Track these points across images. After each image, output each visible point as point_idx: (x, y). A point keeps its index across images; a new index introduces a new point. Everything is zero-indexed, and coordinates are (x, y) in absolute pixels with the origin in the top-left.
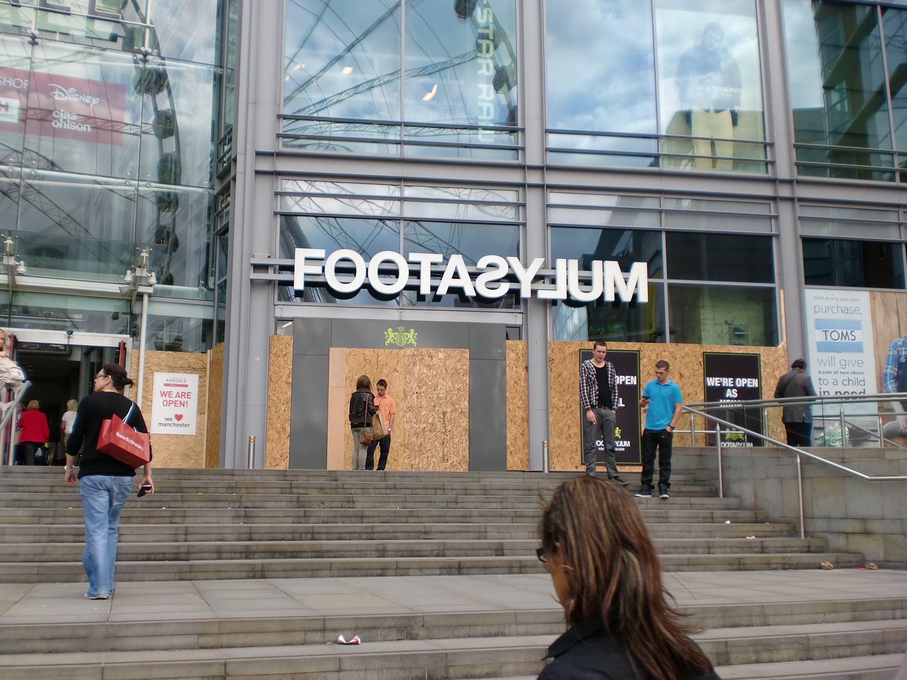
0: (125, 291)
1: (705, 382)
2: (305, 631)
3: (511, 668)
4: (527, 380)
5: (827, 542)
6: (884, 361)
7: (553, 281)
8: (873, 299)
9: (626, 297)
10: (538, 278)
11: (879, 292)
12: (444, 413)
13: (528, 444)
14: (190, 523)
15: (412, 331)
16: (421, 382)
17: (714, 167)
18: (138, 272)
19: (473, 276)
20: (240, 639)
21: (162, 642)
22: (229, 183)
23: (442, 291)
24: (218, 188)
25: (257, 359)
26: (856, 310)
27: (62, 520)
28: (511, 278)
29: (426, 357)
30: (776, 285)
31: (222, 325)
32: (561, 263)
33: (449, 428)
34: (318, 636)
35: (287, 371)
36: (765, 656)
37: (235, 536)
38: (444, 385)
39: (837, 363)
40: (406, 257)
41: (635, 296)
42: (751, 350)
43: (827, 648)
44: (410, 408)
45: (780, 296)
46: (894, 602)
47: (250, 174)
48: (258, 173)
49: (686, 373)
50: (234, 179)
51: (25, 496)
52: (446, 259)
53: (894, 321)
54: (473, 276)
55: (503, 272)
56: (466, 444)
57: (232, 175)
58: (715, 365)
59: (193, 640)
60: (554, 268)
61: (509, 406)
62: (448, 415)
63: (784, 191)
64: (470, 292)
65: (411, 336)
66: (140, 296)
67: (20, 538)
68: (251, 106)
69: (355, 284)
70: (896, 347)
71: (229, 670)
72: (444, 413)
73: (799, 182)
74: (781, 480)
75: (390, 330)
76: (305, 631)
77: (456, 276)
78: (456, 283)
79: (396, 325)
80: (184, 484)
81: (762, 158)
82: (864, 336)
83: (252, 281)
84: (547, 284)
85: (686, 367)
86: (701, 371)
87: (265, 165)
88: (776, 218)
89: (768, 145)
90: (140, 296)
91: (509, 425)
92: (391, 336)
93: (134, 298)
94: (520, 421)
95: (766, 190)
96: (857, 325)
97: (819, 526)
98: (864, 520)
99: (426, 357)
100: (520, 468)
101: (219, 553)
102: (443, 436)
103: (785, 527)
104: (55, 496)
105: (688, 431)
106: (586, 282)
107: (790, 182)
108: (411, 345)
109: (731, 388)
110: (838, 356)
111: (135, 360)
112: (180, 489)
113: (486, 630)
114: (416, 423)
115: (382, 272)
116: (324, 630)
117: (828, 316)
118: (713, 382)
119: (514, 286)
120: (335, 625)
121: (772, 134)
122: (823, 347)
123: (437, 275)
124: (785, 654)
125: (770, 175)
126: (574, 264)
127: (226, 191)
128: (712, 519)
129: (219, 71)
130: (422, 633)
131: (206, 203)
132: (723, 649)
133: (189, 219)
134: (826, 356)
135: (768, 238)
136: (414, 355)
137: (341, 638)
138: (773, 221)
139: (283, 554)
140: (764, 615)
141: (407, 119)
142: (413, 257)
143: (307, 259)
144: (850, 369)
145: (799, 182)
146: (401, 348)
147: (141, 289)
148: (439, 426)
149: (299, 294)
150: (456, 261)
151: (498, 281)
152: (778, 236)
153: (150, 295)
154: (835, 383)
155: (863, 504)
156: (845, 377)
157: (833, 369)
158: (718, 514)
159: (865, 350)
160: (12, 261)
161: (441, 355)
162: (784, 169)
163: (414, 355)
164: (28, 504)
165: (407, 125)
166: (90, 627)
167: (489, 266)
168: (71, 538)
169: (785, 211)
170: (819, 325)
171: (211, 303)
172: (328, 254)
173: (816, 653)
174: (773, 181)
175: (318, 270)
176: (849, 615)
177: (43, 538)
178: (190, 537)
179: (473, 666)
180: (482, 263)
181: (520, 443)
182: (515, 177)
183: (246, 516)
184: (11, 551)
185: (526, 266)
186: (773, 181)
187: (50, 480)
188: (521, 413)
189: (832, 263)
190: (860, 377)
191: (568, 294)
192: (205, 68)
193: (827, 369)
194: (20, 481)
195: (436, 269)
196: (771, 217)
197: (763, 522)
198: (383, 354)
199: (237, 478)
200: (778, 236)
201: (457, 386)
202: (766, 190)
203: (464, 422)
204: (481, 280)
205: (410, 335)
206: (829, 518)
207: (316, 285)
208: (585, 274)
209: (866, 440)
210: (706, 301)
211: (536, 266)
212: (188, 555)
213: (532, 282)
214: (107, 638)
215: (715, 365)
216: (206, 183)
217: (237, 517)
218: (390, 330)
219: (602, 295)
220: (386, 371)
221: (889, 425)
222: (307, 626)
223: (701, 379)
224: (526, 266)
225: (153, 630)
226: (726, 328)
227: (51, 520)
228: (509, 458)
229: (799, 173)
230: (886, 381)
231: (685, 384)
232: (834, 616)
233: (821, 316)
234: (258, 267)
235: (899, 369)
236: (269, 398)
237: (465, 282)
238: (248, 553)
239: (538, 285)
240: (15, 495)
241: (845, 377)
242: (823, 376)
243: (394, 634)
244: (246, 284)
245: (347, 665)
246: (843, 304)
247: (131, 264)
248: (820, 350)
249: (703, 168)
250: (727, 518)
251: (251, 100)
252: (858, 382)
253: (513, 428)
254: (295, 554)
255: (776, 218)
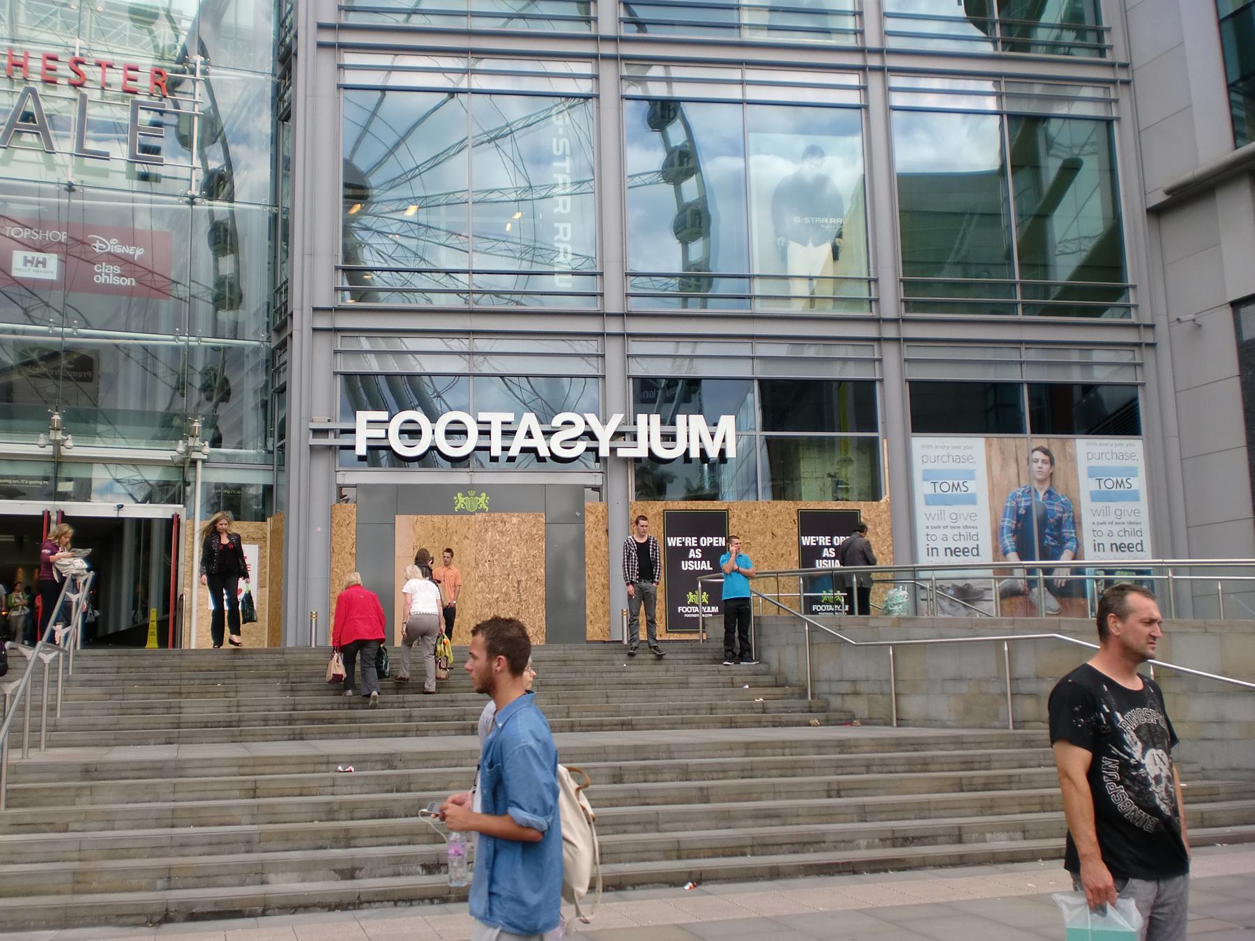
0: (176, 460)
1: (800, 541)
2: (315, 764)
3: (456, 784)
4: (607, 544)
5: (827, 702)
6: (1001, 514)
7: (635, 438)
8: (989, 445)
9: (713, 453)
10: (617, 435)
11: (995, 438)
12: (519, 582)
13: (608, 613)
14: (242, 697)
15: (484, 495)
16: (493, 549)
17: (812, 307)
18: (191, 442)
19: (548, 434)
20: (268, 769)
21: (215, 771)
22: (285, 340)
23: (514, 452)
24: (275, 342)
25: (319, 529)
26: (969, 459)
27: (131, 696)
28: (590, 435)
29: (499, 523)
30: (879, 434)
31: (279, 494)
32: (642, 418)
33: (524, 597)
34: (324, 767)
35: (351, 542)
36: (651, 777)
37: (280, 707)
38: (518, 552)
39: (947, 516)
40: (475, 416)
41: (722, 452)
42: (850, 506)
43: (703, 772)
44: (482, 578)
45: (884, 446)
46: (784, 742)
47: (307, 332)
48: (315, 330)
49: (779, 532)
50: (291, 335)
51: (95, 676)
52: (519, 418)
53: (1013, 470)
54: (548, 434)
55: (579, 429)
56: (542, 614)
57: (288, 332)
58: (811, 522)
59: (235, 770)
60: (635, 423)
61: (589, 572)
62: (523, 584)
63: (890, 331)
64: (544, 453)
65: (483, 500)
66: (194, 462)
67: (96, 712)
68: (307, 258)
69: (420, 448)
70: (1014, 497)
71: (258, 785)
72: (519, 582)
73: (905, 320)
74: (797, 646)
75: (460, 495)
76: (315, 764)
77: (529, 435)
78: (529, 443)
79: (465, 489)
80: (237, 662)
81: (866, 296)
82: (979, 486)
83: (312, 448)
84: (629, 442)
85: (779, 526)
86: (796, 530)
87: (323, 322)
88: (880, 360)
89: (872, 281)
90: (194, 462)
91: (588, 592)
92: (461, 501)
93: (187, 465)
94: (600, 588)
95: (870, 331)
96: (970, 475)
97: (823, 688)
98: (854, 682)
99: (499, 523)
100: (601, 638)
101: (266, 721)
102: (518, 606)
103: (796, 690)
104: (122, 676)
105: (775, 596)
106: (669, 438)
107: (896, 321)
108: (483, 510)
109: (828, 547)
110: (949, 509)
111: (189, 532)
112: (234, 668)
113: (448, 763)
114: (489, 593)
115: (448, 433)
116: (328, 763)
117: (938, 466)
118: (808, 541)
119: (592, 444)
120: (336, 759)
121: (876, 268)
122: (930, 500)
123: (508, 433)
124: (667, 776)
125: (874, 314)
126: (656, 419)
127: (283, 346)
128: (732, 684)
129: (274, 210)
130: (400, 765)
131: (263, 356)
132: (617, 772)
133: (246, 370)
134: (934, 509)
135: (870, 384)
136: (485, 521)
137: (340, 768)
138: (877, 364)
139: (322, 721)
140: (670, 751)
141: (475, 268)
142: (483, 417)
143: (369, 422)
144: (961, 523)
145: (905, 320)
146: (473, 514)
147: (195, 455)
148: (514, 596)
149: (361, 458)
150: (529, 420)
151: (576, 439)
152: (881, 381)
153: (204, 461)
154: (945, 538)
155: (855, 667)
156: (956, 531)
157: (942, 523)
158: (737, 679)
159: (978, 501)
160: (59, 436)
161: (515, 520)
162: (890, 306)
163: (485, 521)
164: (99, 683)
165: (474, 272)
166: (165, 761)
167: (564, 423)
168: (140, 711)
169: (891, 354)
170: (927, 476)
171: (270, 467)
172: (391, 417)
173: (694, 776)
174: (878, 321)
175: (382, 434)
176: (743, 752)
177: (116, 712)
178: (242, 709)
179: (429, 783)
180: (557, 421)
181: (600, 611)
182: (593, 326)
183: (292, 690)
184: (91, 722)
185: (605, 422)
186: (878, 321)
187: (115, 662)
188: (601, 580)
189: (941, 409)
190: (973, 532)
191: (650, 450)
192: (258, 207)
193: (936, 523)
194: (90, 663)
195: (507, 428)
196: (874, 360)
197: (783, 686)
198: (453, 520)
199: (287, 657)
200: (881, 381)
201: (533, 552)
202: (870, 331)
203: (541, 591)
204: (556, 440)
205: (482, 500)
206: (829, 681)
207: (378, 454)
208: (669, 429)
209: (979, 600)
210: (802, 452)
211: (615, 422)
212: (239, 722)
213: (612, 439)
214: (176, 769)
215: (811, 522)
216: (263, 336)
217: (284, 691)
218: (460, 495)
219: (687, 450)
220: (456, 539)
221: (1006, 583)
222: (316, 760)
223: (796, 539)
224: (605, 422)
225: (208, 763)
226: (829, 481)
227: (120, 697)
228: (589, 627)
229: (907, 310)
230: (1002, 535)
231: (778, 544)
232: (730, 752)
233: (929, 466)
234: (317, 432)
235: (1018, 521)
236: (332, 570)
237: (539, 442)
238: (291, 720)
239: (619, 443)
240: (87, 676)
241: (956, 531)
242: (931, 532)
243: (379, 766)
244: (305, 451)
245: (338, 782)
246: (955, 453)
247: (182, 433)
248: (927, 504)
249: (797, 308)
250: (746, 683)
251: (307, 251)
252: (971, 537)
253: (594, 596)
254: (331, 721)
255: (880, 360)
